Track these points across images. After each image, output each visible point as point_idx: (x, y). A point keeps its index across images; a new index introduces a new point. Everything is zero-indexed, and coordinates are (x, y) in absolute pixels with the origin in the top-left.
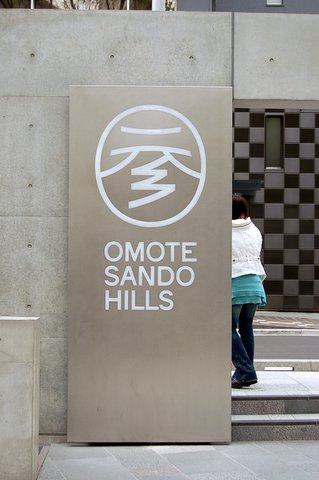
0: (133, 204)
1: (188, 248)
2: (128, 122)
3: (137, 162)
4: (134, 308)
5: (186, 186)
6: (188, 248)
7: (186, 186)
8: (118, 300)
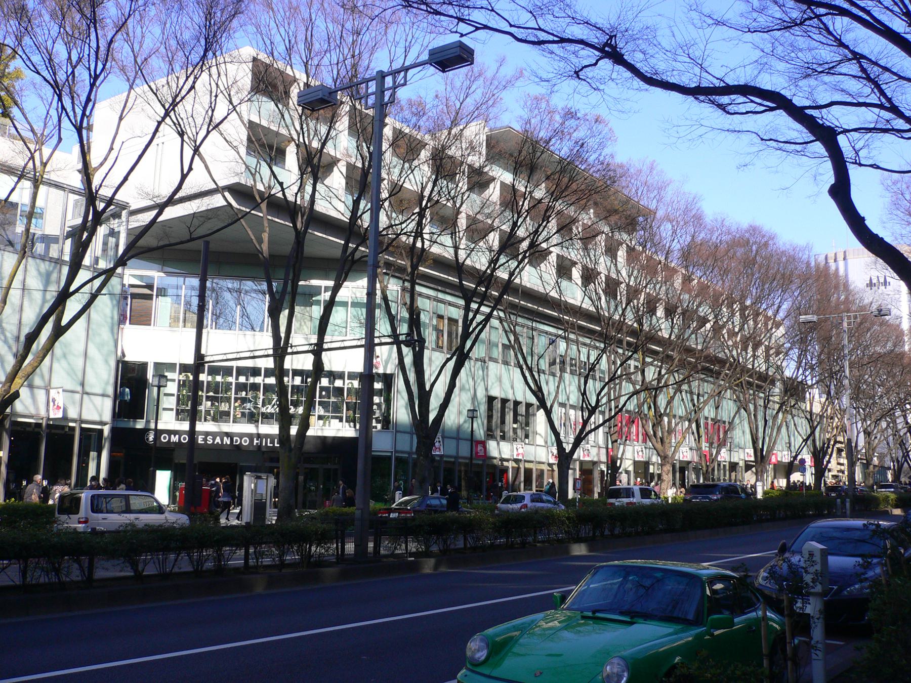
4: (269, 445)
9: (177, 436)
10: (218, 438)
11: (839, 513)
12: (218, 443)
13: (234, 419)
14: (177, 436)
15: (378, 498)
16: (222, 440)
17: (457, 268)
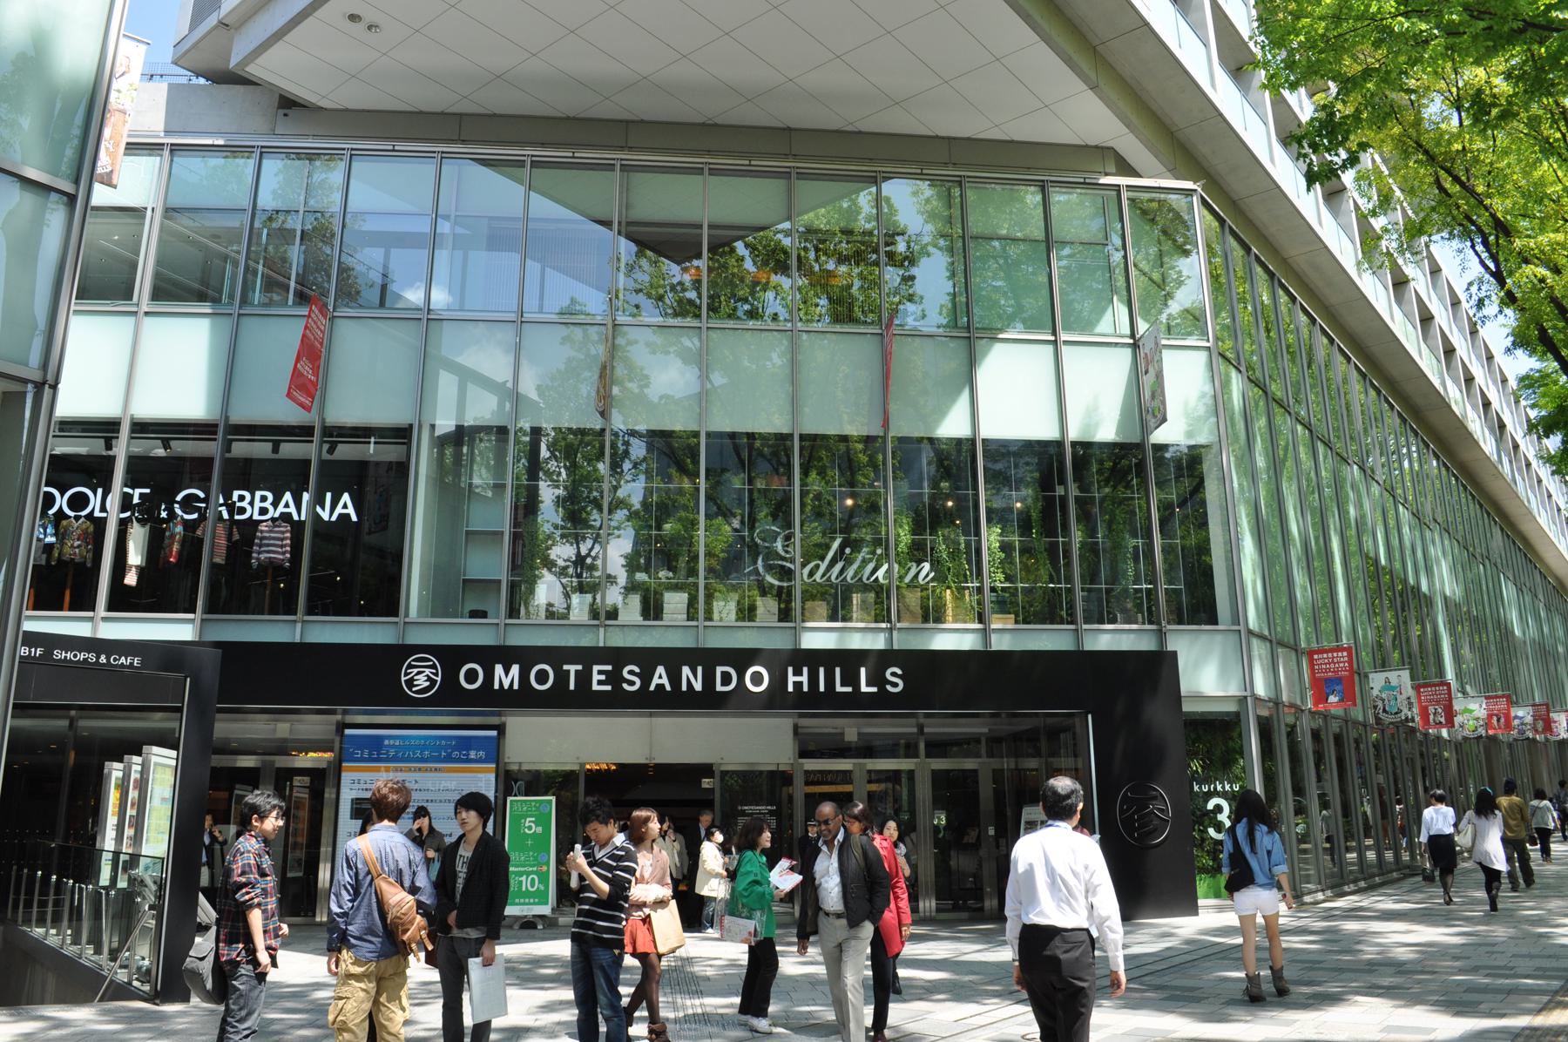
0: (414, 689)
1: (600, 672)
2: (414, 660)
3: (417, 674)
4: (839, 689)
5: (433, 682)
6: (600, 672)
7: (433, 682)
8: (804, 679)
9: (515, 669)
10: (660, 670)
11: (709, 512)
12: (660, 687)
13: (327, 602)
14: (515, 669)
15: (1550, 66)
16: (675, 677)
17: (1397, 627)
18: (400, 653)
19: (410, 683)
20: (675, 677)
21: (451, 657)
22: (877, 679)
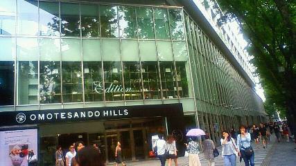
14: (43, 115)
18: (15, 113)
19: (18, 120)
20: (73, 115)
21: (28, 114)
22: (122, 112)
